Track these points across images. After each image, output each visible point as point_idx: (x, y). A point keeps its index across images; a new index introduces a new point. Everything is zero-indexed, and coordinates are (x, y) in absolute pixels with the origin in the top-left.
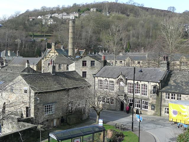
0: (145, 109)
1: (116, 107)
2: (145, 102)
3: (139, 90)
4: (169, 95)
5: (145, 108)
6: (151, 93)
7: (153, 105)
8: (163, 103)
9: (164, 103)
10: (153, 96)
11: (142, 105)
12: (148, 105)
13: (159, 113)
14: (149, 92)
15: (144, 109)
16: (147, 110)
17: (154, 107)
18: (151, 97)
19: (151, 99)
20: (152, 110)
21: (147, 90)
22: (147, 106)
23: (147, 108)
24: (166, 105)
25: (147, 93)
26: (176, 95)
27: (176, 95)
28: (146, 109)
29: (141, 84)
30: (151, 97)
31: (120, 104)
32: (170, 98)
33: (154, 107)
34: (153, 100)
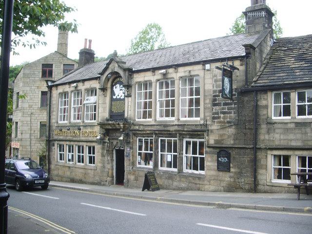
0: (195, 172)
1: (102, 172)
2: (195, 144)
3: (161, 97)
4: (287, 99)
5: (195, 168)
6: (215, 105)
7: (222, 151)
8: (264, 137)
9: (267, 137)
10: (224, 113)
11: (85, 113)
12: (207, 153)
13: (246, 180)
14: (208, 101)
15: (190, 171)
16: (202, 172)
17: (228, 156)
18: (214, 118)
19: (215, 127)
20: (221, 173)
21: (201, 97)
22: (202, 160)
23: (202, 168)
24: (277, 143)
25: (201, 107)
26: (294, 96)
27: (294, 96)
28: (199, 172)
29: (86, 90)
30: (214, 118)
31: (112, 160)
32: (295, 110)
33: (229, 158)
34: (222, 132)
